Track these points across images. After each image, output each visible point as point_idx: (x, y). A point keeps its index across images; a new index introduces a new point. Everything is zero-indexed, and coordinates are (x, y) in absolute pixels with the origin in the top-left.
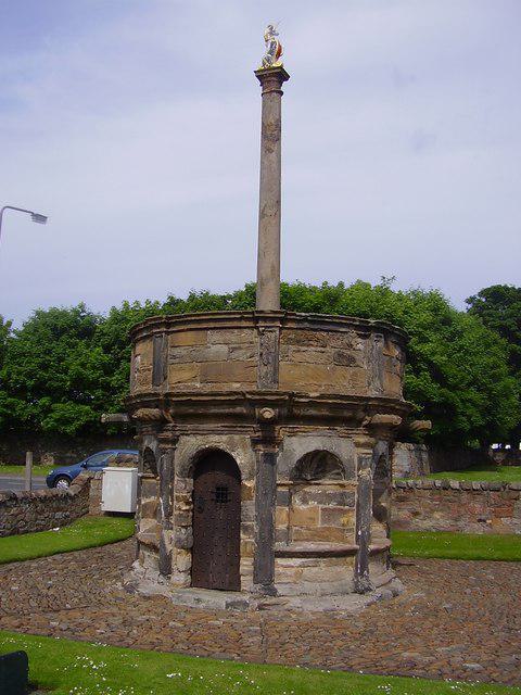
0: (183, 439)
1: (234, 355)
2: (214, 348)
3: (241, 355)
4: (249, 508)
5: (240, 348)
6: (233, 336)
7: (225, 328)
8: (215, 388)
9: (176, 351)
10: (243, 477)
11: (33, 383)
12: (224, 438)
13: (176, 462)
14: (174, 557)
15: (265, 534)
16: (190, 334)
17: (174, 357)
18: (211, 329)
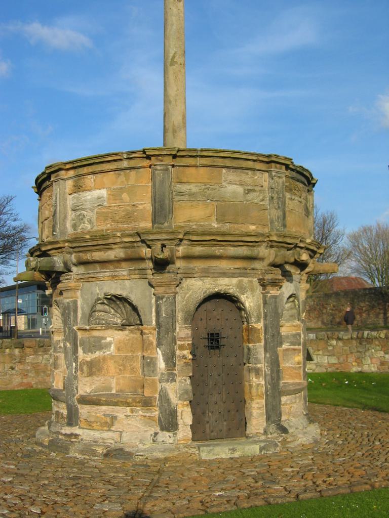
0: (187, 283)
1: (250, 196)
2: (231, 188)
3: (254, 197)
4: (259, 349)
5: (254, 191)
6: (248, 177)
7: (242, 168)
8: (227, 227)
9: (184, 188)
10: (370, 332)
11: (216, 226)
12: (235, 281)
13: (178, 307)
14: (179, 411)
15: (275, 375)
16: (202, 170)
17: (181, 194)
18: (228, 167)
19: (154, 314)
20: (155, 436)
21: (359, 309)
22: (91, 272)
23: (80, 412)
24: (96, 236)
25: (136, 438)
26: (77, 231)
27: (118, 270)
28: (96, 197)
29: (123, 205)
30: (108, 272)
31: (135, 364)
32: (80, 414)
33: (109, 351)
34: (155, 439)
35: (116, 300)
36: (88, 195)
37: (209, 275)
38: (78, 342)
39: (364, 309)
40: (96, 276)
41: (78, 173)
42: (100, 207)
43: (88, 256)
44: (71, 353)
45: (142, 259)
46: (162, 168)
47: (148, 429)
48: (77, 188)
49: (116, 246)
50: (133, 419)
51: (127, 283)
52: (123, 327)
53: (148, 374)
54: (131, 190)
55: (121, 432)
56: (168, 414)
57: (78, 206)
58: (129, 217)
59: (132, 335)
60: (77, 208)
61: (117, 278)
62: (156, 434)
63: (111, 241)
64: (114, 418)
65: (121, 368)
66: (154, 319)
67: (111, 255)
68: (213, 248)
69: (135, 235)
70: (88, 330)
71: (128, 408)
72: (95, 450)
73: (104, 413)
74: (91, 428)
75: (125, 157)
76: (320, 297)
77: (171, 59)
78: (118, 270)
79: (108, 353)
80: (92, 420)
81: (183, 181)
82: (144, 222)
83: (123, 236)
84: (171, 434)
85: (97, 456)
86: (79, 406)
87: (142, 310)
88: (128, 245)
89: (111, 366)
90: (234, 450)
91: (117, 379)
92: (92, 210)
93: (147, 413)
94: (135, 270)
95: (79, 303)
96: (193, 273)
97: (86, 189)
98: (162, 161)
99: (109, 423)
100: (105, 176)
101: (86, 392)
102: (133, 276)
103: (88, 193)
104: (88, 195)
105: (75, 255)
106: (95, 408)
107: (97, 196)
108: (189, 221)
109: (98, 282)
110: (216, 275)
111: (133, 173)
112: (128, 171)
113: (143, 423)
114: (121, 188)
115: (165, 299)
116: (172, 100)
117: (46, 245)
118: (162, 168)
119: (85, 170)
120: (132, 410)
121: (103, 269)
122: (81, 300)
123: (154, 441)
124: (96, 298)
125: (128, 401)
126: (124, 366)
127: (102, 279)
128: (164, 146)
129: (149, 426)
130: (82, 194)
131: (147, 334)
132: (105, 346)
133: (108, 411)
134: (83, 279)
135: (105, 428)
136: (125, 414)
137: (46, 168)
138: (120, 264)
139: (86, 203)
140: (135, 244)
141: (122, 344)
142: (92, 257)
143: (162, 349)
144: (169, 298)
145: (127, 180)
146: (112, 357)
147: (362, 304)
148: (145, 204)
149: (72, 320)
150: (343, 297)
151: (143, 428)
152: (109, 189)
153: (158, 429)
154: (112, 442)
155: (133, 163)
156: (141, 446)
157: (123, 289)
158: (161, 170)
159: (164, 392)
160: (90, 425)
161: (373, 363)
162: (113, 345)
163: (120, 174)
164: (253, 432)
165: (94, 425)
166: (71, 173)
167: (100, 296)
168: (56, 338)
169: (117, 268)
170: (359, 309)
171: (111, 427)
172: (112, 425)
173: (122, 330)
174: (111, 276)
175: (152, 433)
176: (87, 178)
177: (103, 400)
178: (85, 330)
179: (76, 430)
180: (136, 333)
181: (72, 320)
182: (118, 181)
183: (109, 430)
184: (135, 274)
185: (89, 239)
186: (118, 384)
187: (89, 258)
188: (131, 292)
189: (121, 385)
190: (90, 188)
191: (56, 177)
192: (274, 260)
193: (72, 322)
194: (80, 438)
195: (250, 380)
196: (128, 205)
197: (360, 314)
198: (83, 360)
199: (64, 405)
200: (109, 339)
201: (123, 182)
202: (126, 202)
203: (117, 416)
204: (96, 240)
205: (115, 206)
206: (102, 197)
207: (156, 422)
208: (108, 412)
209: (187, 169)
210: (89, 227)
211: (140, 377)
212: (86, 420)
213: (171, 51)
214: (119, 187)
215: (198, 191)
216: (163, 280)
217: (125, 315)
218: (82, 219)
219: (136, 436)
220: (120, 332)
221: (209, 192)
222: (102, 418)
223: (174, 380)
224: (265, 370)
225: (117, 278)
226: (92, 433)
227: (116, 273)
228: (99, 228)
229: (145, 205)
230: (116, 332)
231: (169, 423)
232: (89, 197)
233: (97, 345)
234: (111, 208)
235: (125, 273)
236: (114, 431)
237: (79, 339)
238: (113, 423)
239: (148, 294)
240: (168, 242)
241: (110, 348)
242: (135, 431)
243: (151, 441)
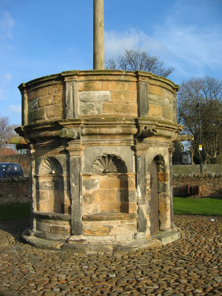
16: (158, 88)
19: (134, 166)
20: (135, 236)
21: (23, 164)
23: (84, 225)
24: (109, 119)
25: (125, 238)
27: (115, 140)
28: (103, 95)
29: (121, 102)
30: (107, 140)
31: (112, 195)
32: (83, 227)
33: (97, 188)
34: (136, 237)
36: (96, 93)
38: (82, 183)
39: (26, 164)
40: (98, 142)
41: (88, 78)
42: (105, 101)
43: (94, 130)
45: (130, 134)
46: (144, 83)
47: (131, 232)
48: (87, 88)
49: (119, 126)
50: (123, 227)
53: (131, 200)
54: (126, 94)
55: (115, 236)
56: (143, 222)
57: (88, 99)
58: (125, 109)
59: (110, 178)
60: (87, 100)
61: (113, 145)
62: (136, 234)
63: (118, 122)
64: (110, 228)
65: (103, 197)
66: (134, 169)
67: (114, 130)
68: (163, 131)
69: (133, 120)
71: (119, 221)
72: (107, 248)
73: (103, 225)
74: (94, 235)
75: (124, 74)
76: (2, 157)
77: (100, 23)
78: (115, 140)
79: (96, 189)
80: (95, 230)
82: (133, 113)
83: (126, 120)
84: (143, 234)
85: (109, 252)
86: (83, 222)
87: (127, 164)
88: (126, 125)
89: (98, 197)
90: (172, 238)
91: (101, 204)
92: (99, 102)
93: (130, 223)
94: (125, 140)
95: (83, 159)
96: (152, 144)
97: (95, 89)
98: (144, 79)
99: (108, 230)
100: (109, 83)
101: (89, 213)
102: (123, 144)
103: (96, 92)
104: (96, 93)
105: (86, 129)
106: (96, 222)
107: (103, 95)
108: (153, 115)
109: (99, 147)
110: (159, 145)
111: (127, 84)
112: (124, 82)
113: (128, 229)
114: (120, 92)
115: (141, 158)
116: (100, 46)
117: (67, 121)
118: (144, 83)
119: (95, 78)
120: (122, 222)
121: (103, 139)
122: (85, 157)
123: (135, 238)
124: (97, 156)
125: (122, 217)
126: (104, 196)
127: (102, 145)
128: (94, 69)
129: (132, 230)
131: (130, 178)
132: (95, 185)
133: (106, 223)
135: (105, 234)
136: (118, 224)
137: (63, 72)
138: (115, 136)
140: (131, 125)
141: (103, 184)
142: (100, 131)
143: (140, 186)
144: (143, 157)
145: (124, 87)
146: (98, 191)
147: (25, 162)
148: (133, 102)
150: (15, 158)
151: (128, 231)
152: (111, 91)
153: (136, 232)
154: (110, 241)
155: (127, 78)
156: (128, 242)
157: (115, 151)
158: (143, 84)
159: (141, 210)
160: (92, 233)
162: (98, 184)
163: (119, 84)
164: (166, 228)
165: (96, 233)
166: (82, 78)
168: (42, 180)
169: (113, 138)
170: (23, 164)
171: (109, 233)
172: (110, 231)
173: (103, 175)
175: (133, 234)
176: (96, 82)
177: (105, 218)
179: (82, 237)
180: (112, 177)
182: (118, 88)
183: (108, 235)
184: (124, 143)
185: (104, 120)
186: (101, 207)
187: (97, 132)
188: (121, 153)
189: (103, 207)
190: (98, 89)
191: (69, 79)
192: (176, 139)
194: (87, 242)
195: (166, 201)
196: (124, 102)
197: (24, 166)
198: (86, 194)
201: (121, 88)
202: (123, 100)
203: (113, 226)
204: (109, 121)
205: (115, 102)
206: (107, 95)
207: (136, 227)
208: (106, 225)
209: (152, 86)
210: (97, 113)
211: (116, 202)
212: (89, 230)
213: (100, 18)
214: (118, 91)
215: (157, 99)
216: (143, 147)
217: (107, 167)
218: (92, 107)
219: (124, 237)
220: (102, 177)
221: (160, 100)
222: (102, 228)
223: (144, 203)
224: (170, 195)
225: (113, 145)
226: (95, 238)
227: (113, 142)
228: (105, 114)
229: (133, 103)
230: (100, 176)
231: (141, 228)
232: (97, 95)
234: (113, 103)
235: (119, 142)
236: (111, 235)
237: (82, 181)
238: (110, 231)
239: (130, 154)
240: (148, 125)
241: (97, 186)
242: (123, 234)
243: (133, 238)
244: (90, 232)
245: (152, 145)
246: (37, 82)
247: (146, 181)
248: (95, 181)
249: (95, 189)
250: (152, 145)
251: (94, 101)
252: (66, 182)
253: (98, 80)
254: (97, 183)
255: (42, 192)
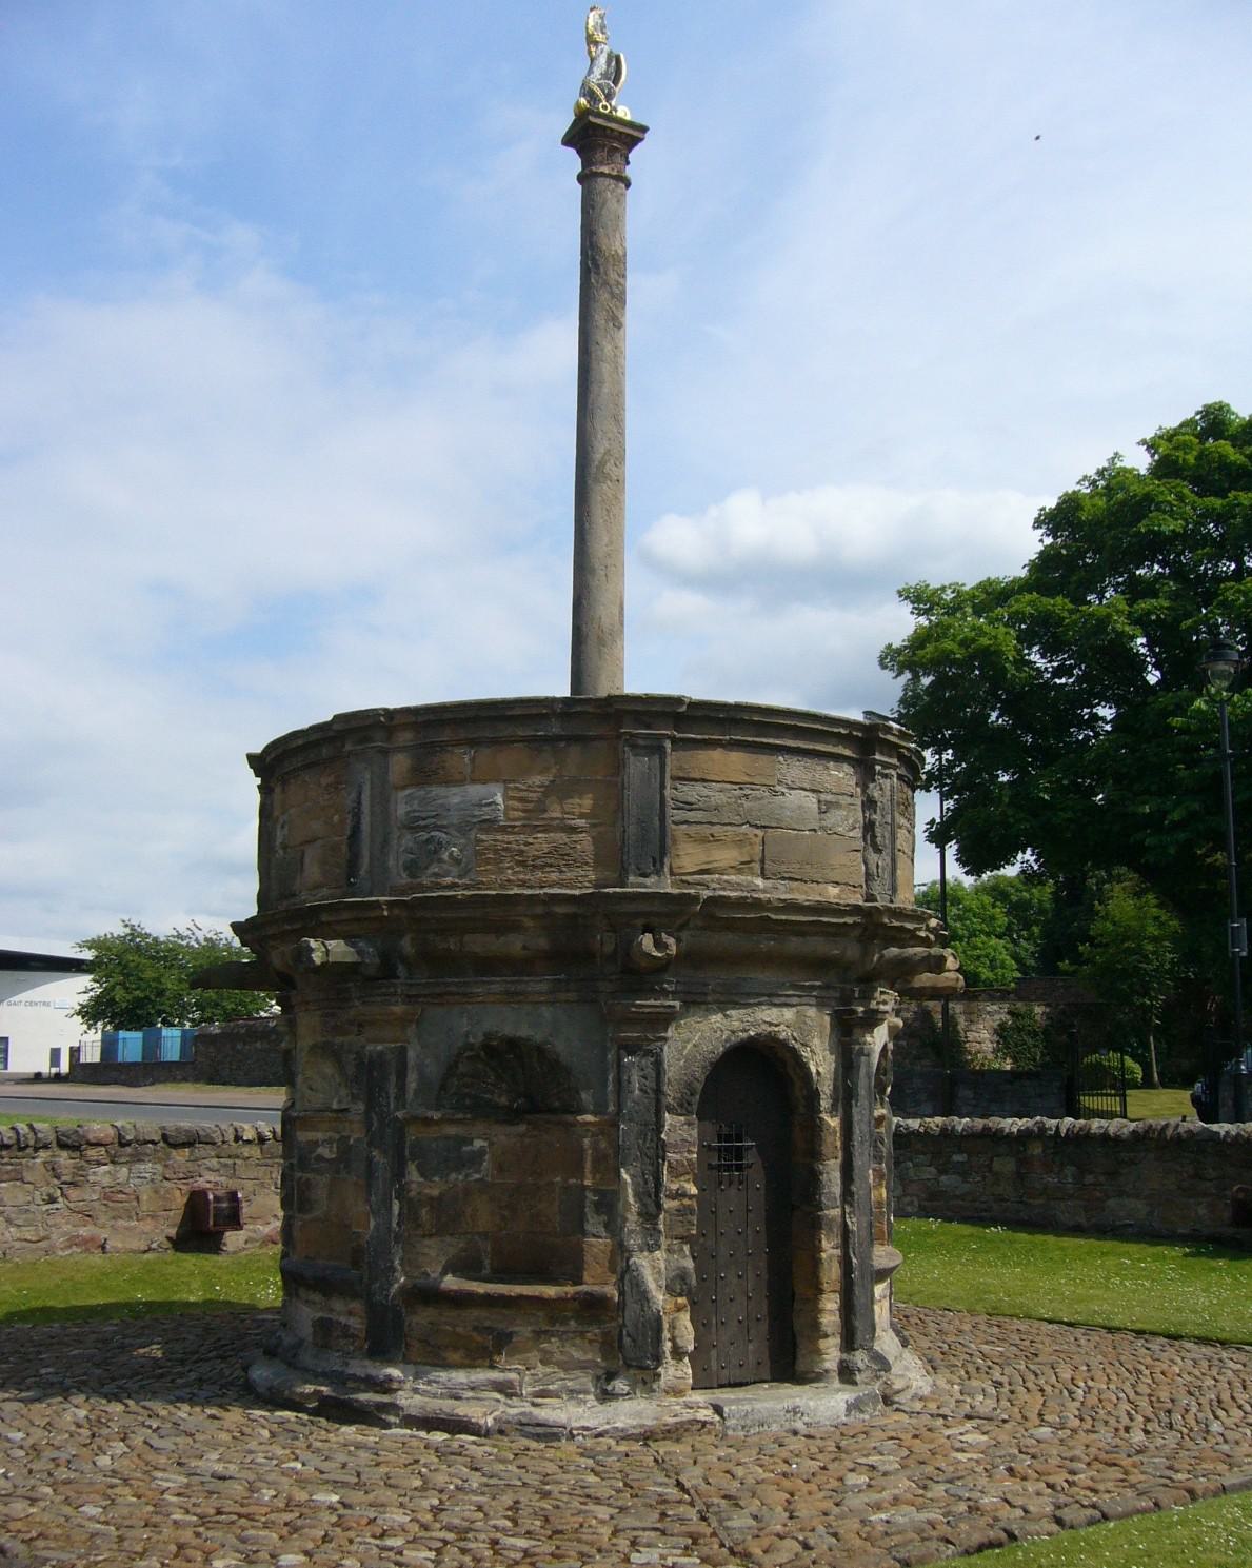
5: (837, 805)
22: (450, 980)
26: (419, 880)
35: (503, 1054)
37: (776, 1001)
44: (388, 1175)
46: (648, 742)
48: (423, 775)
51: (546, 1012)
52: (512, 1116)
57: (424, 819)
67: (515, 944)
70: (437, 1123)
78: (526, 979)
79: (477, 1176)
81: (692, 775)
95: (411, 1054)
102: (563, 996)
103: (455, 790)
105: (412, 939)
109: (469, 1007)
111: (575, 751)
119: (446, 735)
122: (418, 1047)
130: (436, 791)
134: (425, 996)
139: (445, 813)
149: (392, 1097)
161: (911, 1195)
167: (471, 1040)
174: (507, 993)
178: (428, 1122)
181: (392, 1097)
193: (392, 1099)
199: (356, 1305)
200: (478, 1143)
221: (747, 804)
225: (521, 998)
227: (520, 987)
232: (456, 800)
233: (457, 1158)
244: (429, 1349)
245: (709, 999)
246: (579, 709)
247: (664, 1152)
248: (471, 1143)
249: (467, 1176)
250: (709, 999)
251: (445, 827)
252: (826, 1150)
253: (458, 743)
254: (481, 1152)
255: (308, 1180)
